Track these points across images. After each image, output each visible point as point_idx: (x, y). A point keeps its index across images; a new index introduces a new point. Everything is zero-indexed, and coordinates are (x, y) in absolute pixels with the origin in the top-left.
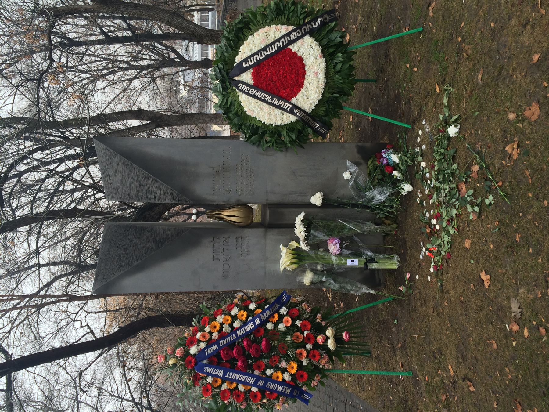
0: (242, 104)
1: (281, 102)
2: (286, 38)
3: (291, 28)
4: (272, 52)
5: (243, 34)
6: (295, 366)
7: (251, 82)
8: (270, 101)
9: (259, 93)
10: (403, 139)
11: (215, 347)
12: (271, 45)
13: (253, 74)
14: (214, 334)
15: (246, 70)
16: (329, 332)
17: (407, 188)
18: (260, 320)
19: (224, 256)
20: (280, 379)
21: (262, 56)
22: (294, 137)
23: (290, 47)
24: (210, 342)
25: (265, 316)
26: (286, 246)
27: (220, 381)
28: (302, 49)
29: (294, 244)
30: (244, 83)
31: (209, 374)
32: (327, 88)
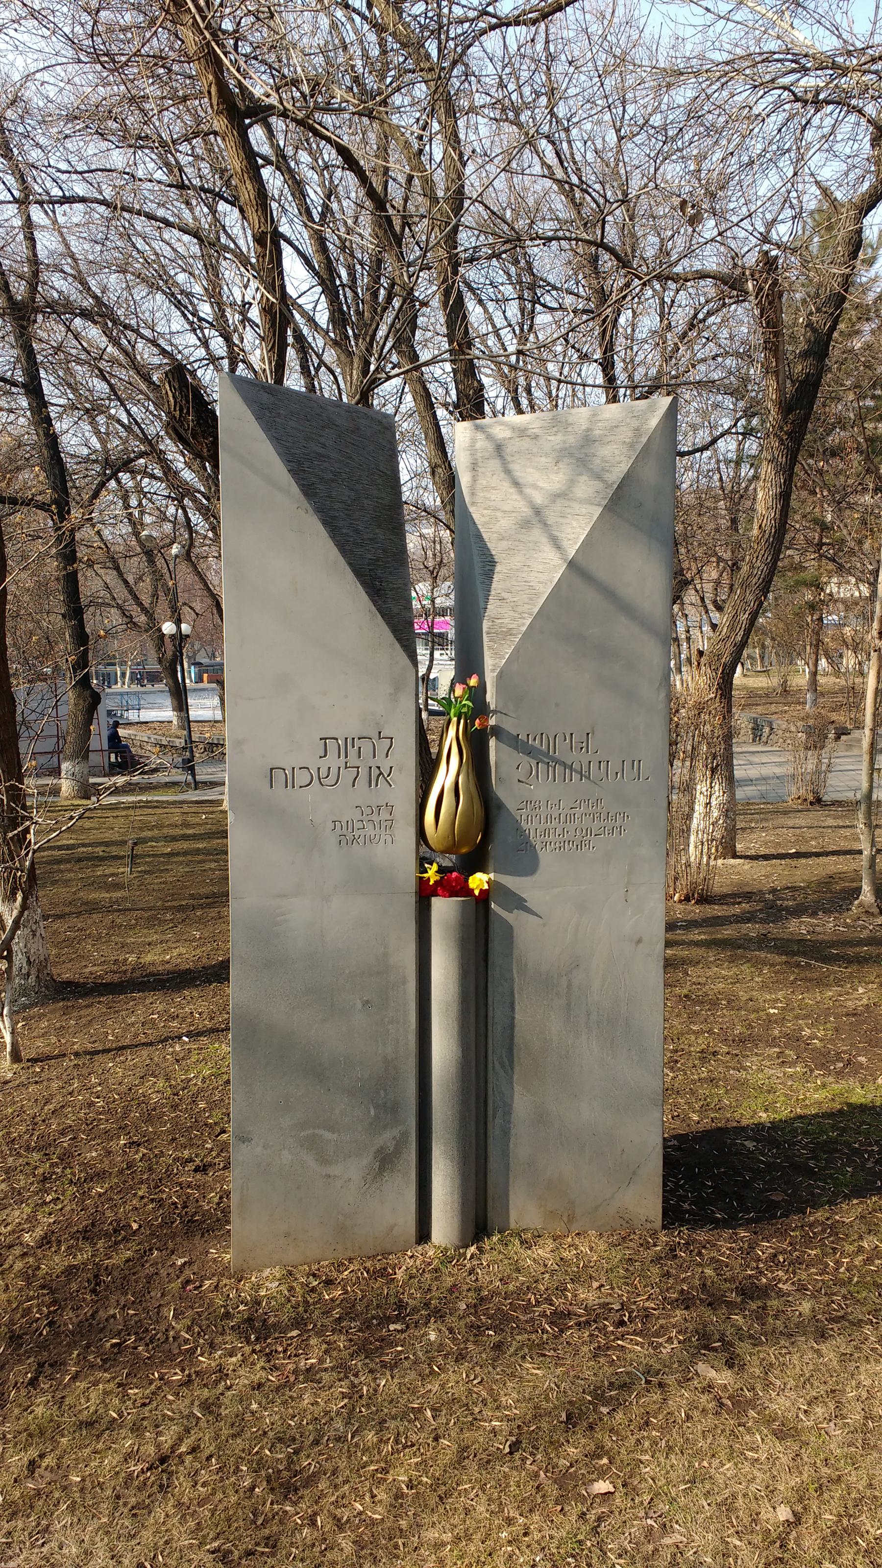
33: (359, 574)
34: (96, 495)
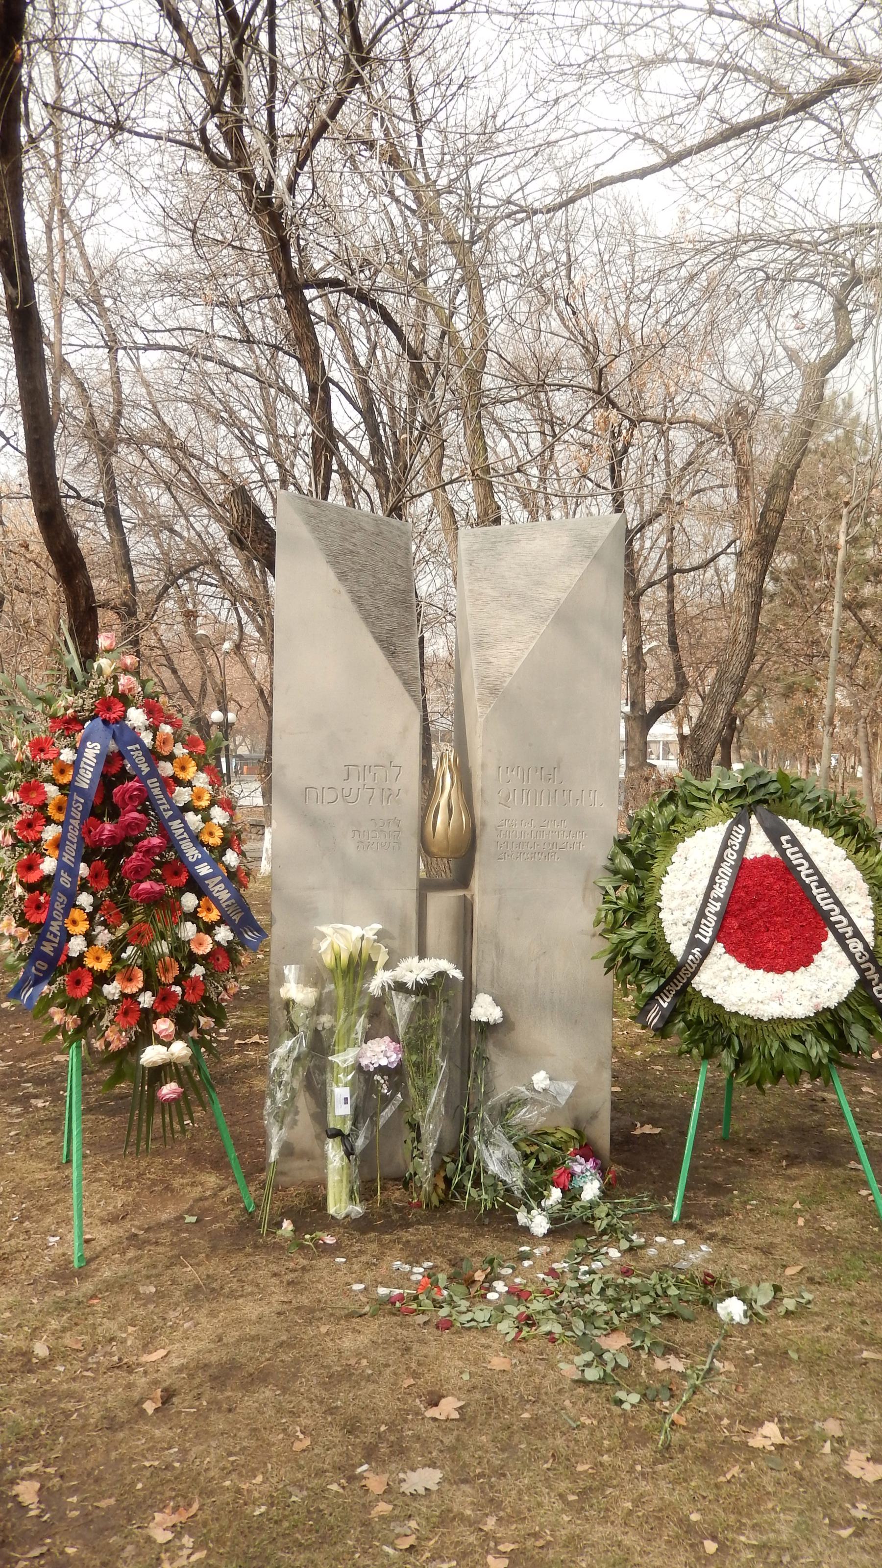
0: (699, 832)
1: (713, 919)
2: (850, 929)
3: (869, 938)
4: (818, 898)
5: (846, 836)
6: (104, 964)
7: (749, 855)
8: (712, 894)
9: (729, 871)
10: (638, 1205)
11: (145, 769)
12: (833, 896)
13: (766, 857)
14: (168, 764)
15: (777, 844)
16: (180, 1049)
17: (540, 1224)
18: (208, 877)
19: (354, 791)
20: (72, 929)
21: (808, 876)
22: (637, 949)
23: (830, 935)
24: (154, 756)
25: (217, 888)
26: (381, 935)
27: (65, 779)
28: (829, 963)
29: (382, 958)
30: (746, 836)
31: (79, 752)
32: (749, 1022)
33: (379, 640)
34: (160, 597)
